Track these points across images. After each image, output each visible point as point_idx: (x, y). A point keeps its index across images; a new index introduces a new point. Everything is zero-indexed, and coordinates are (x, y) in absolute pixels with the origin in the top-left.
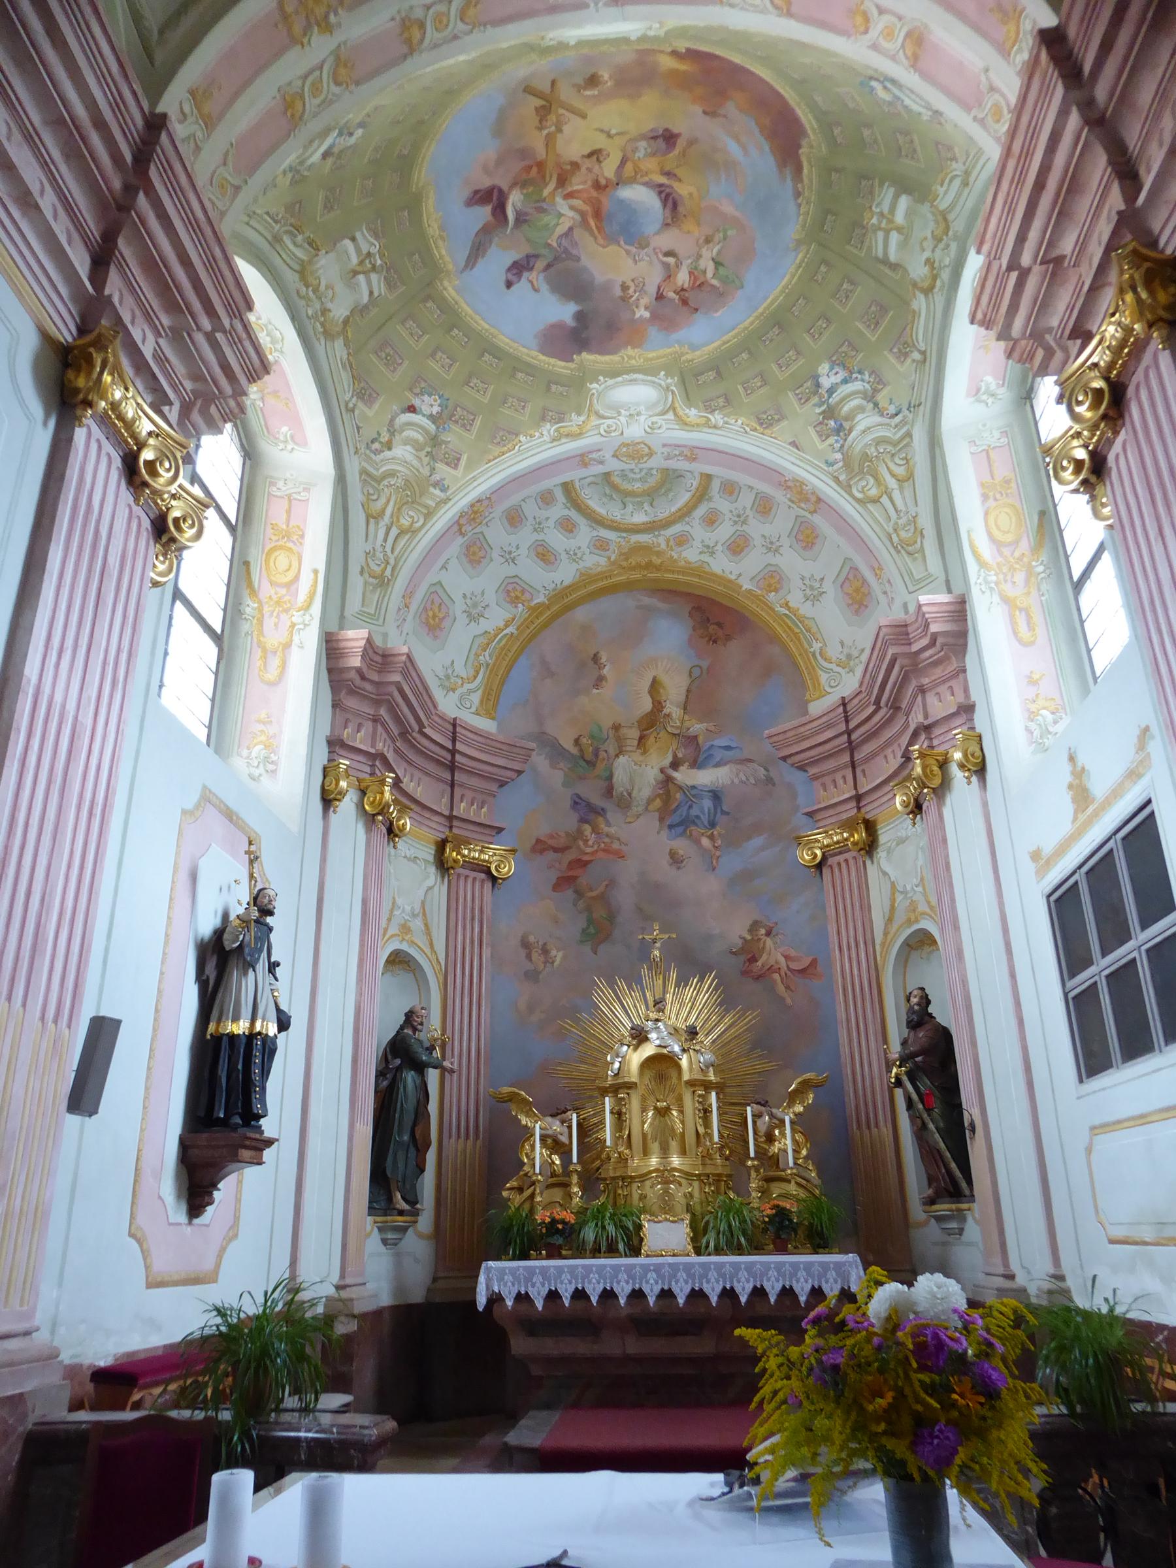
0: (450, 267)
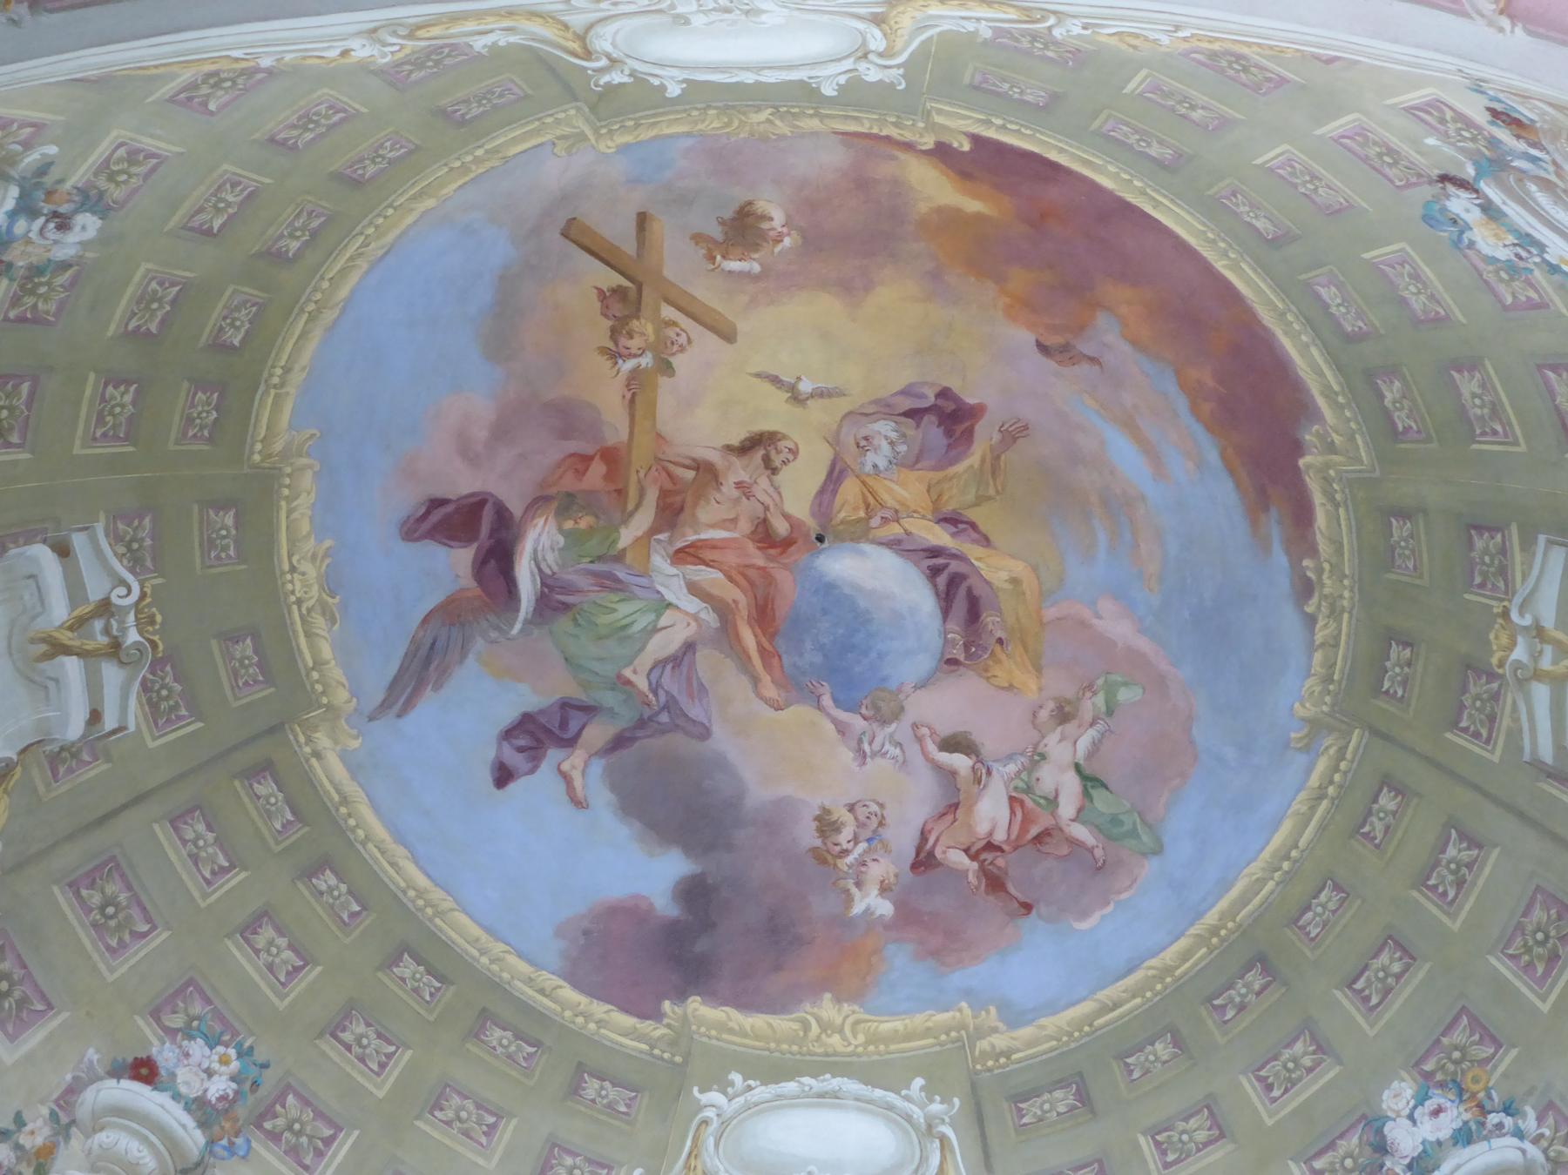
0: (341, 696)
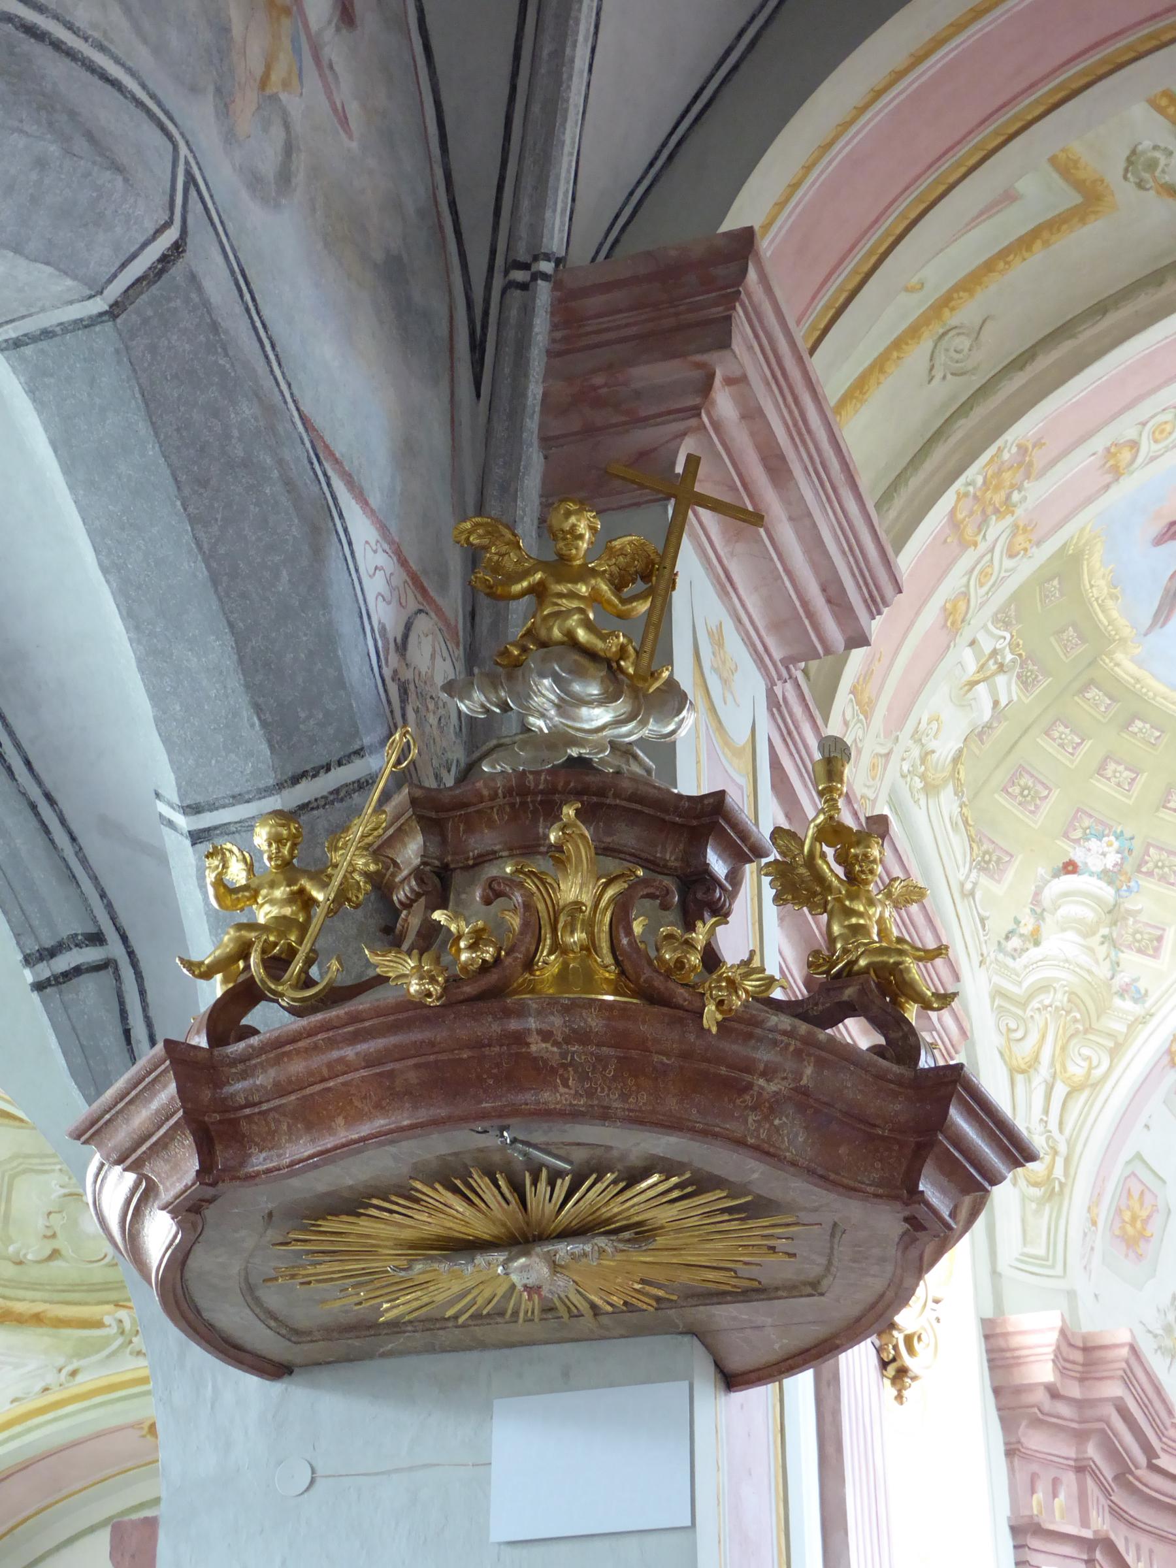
0: (1127, 632)
